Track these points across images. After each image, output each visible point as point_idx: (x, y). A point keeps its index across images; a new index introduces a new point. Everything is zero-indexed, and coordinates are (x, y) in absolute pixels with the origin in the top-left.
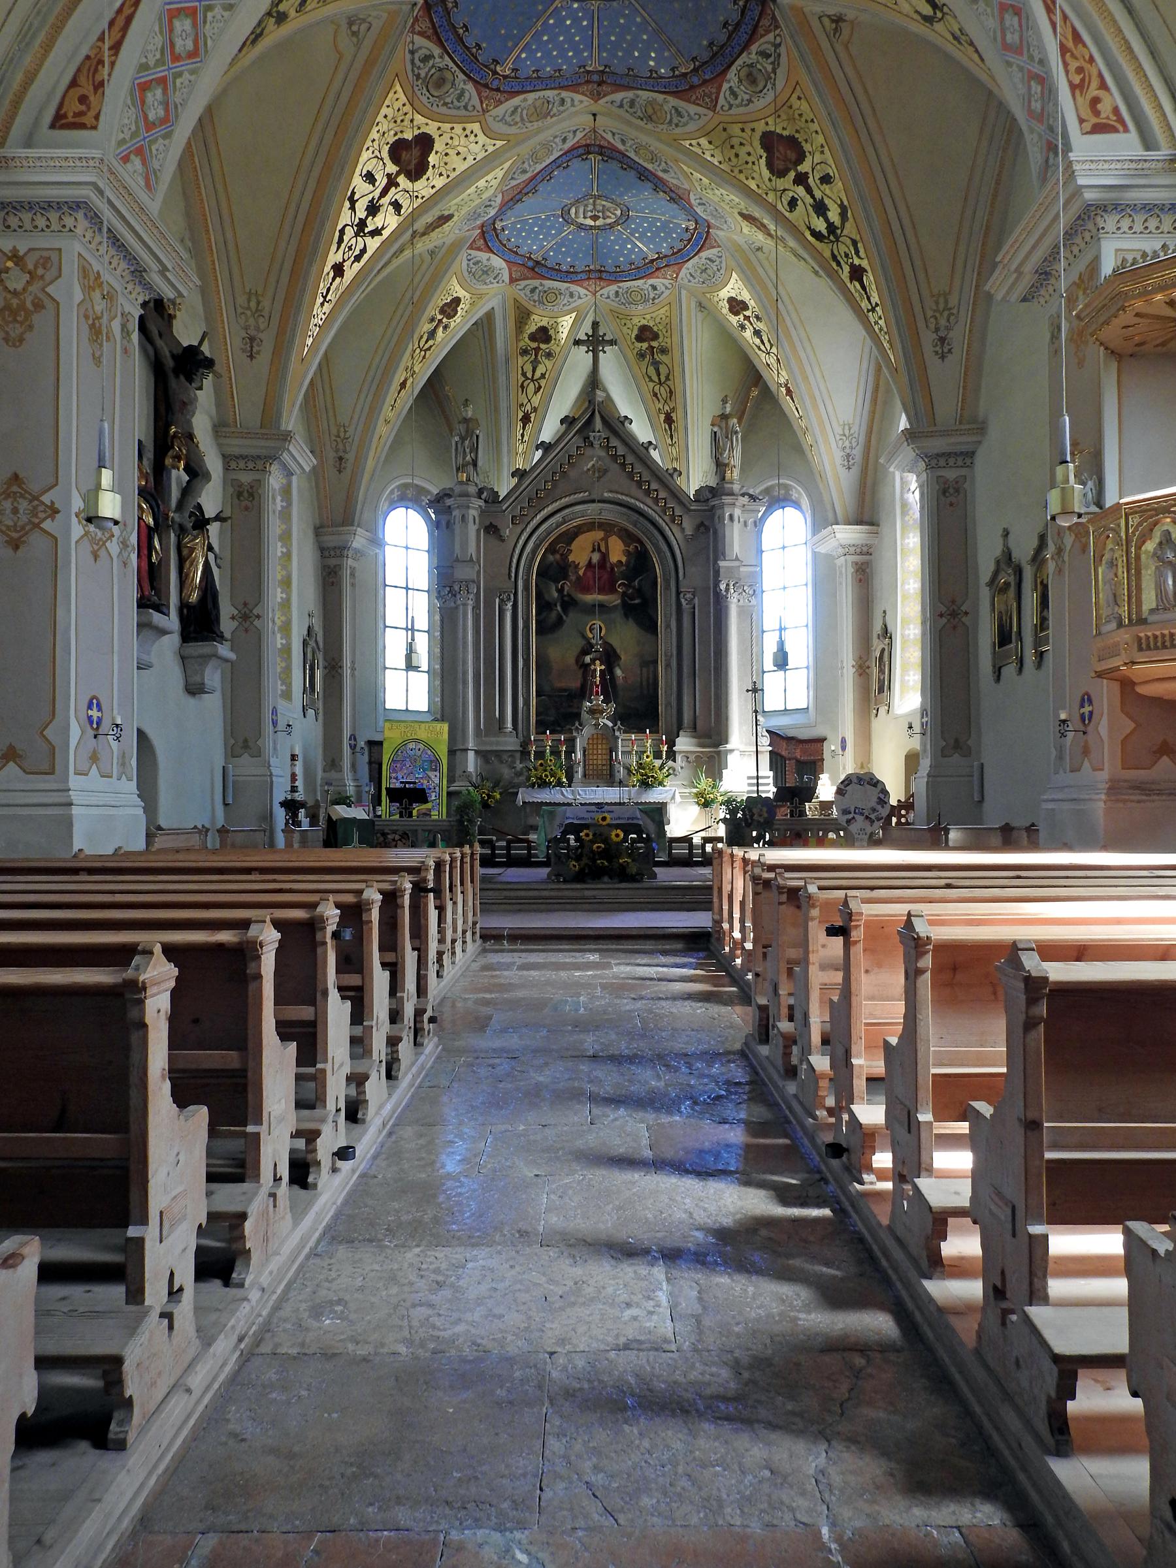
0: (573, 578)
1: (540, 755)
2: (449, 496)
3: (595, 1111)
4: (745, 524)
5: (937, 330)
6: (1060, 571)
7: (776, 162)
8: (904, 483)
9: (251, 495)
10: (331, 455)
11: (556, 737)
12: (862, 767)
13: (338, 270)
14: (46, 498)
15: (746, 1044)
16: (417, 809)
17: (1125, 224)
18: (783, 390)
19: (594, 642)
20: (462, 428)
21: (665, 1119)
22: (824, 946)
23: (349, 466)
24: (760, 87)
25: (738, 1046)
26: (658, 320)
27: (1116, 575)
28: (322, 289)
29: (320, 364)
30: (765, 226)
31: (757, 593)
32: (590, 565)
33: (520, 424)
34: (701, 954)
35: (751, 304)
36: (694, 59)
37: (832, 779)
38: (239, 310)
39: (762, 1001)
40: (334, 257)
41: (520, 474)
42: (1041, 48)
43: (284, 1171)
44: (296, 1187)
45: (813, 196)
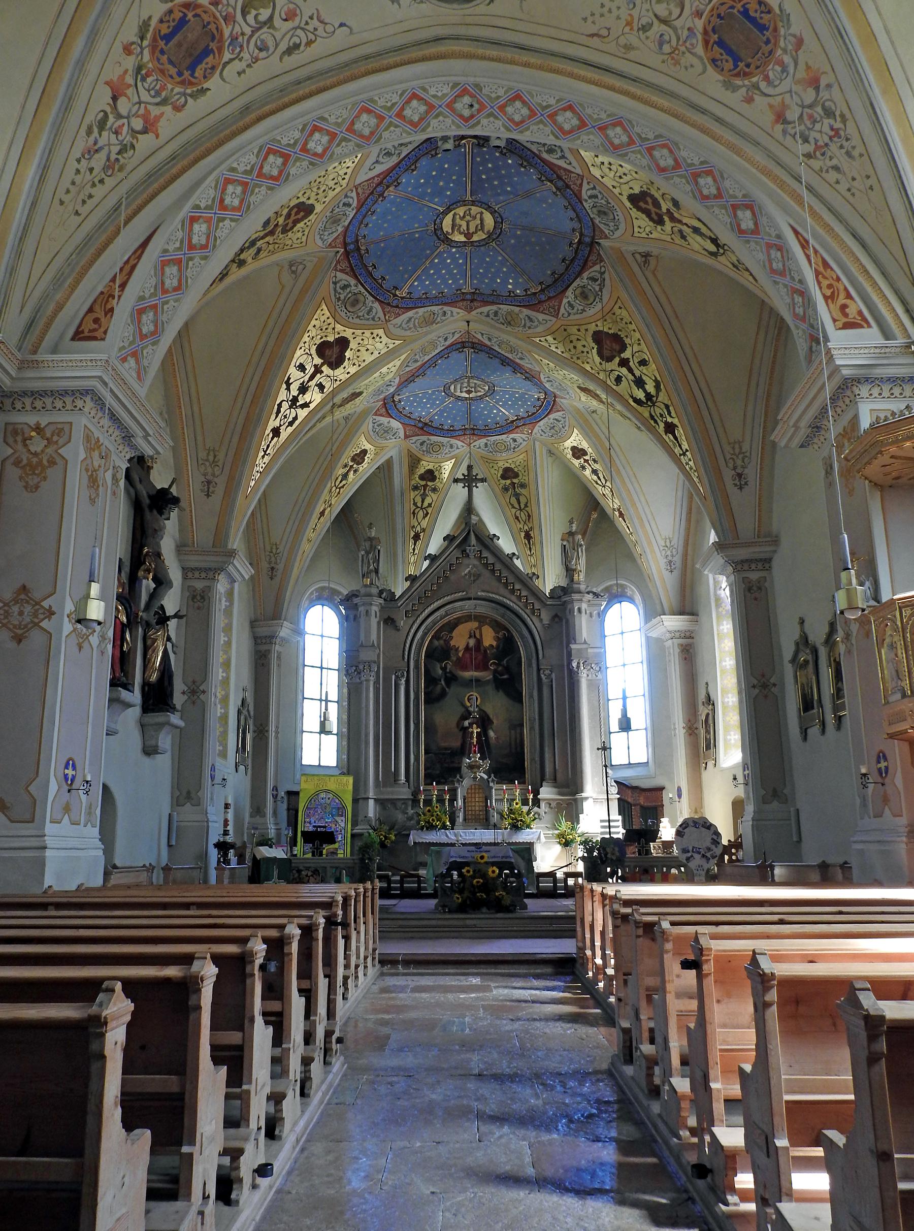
0: (454, 659)
1: (428, 802)
2: (357, 596)
3: (483, 1128)
4: (591, 616)
5: (735, 468)
6: (849, 652)
7: (605, 351)
8: (716, 583)
9: (203, 597)
10: (265, 565)
11: (441, 787)
12: (696, 812)
13: (276, 432)
14: (45, 604)
15: (612, 1064)
16: (327, 848)
17: (876, 391)
18: (617, 513)
19: (471, 709)
20: (368, 544)
21: (545, 1137)
22: (678, 976)
23: (279, 574)
24: (592, 300)
25: (605, 1066)
26: (518, 463)
27: (896, 655)
28: (264, 445)
29: (259, 500)
30: (598, 396)
31: (601, 668)
32: (467, 648)
33: (412, 541)
34: (568, 978)
35: (590, 450)
36: (541, 283)
37: (672, 823)
38: (200, 462)
39: (625, 1024)
40: (273, 423)
41: (412, 579)
42: (800, 271)
43: (212, 1190)
44: (221, 1204)
45: (633, 375)
